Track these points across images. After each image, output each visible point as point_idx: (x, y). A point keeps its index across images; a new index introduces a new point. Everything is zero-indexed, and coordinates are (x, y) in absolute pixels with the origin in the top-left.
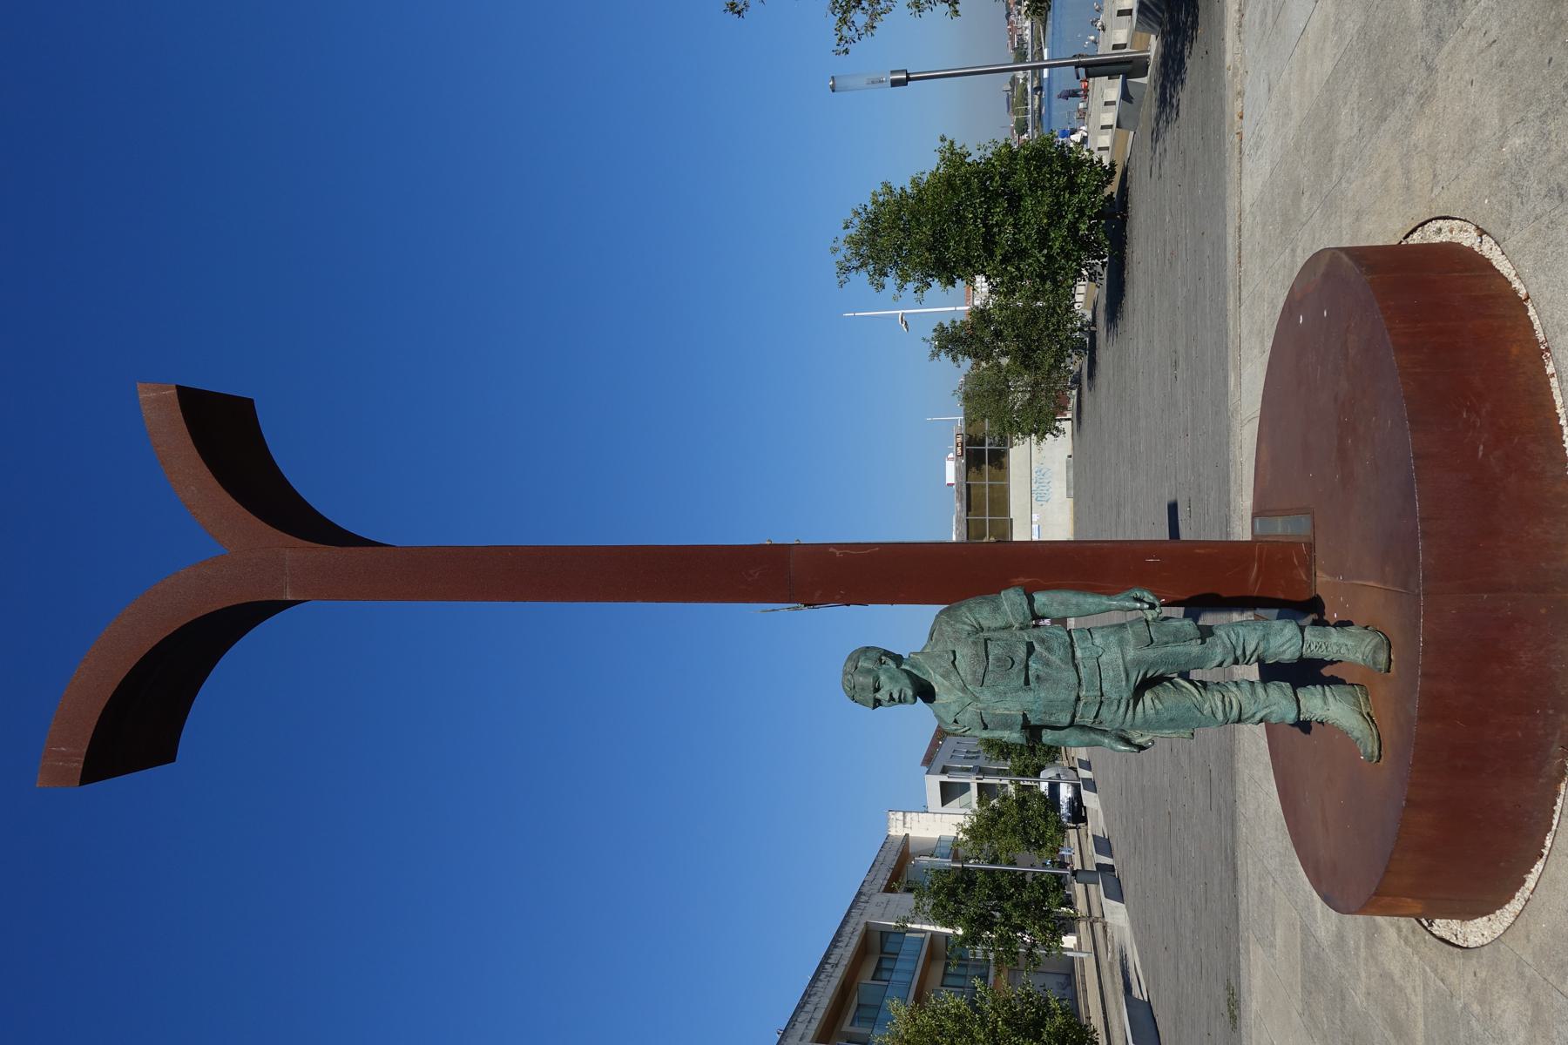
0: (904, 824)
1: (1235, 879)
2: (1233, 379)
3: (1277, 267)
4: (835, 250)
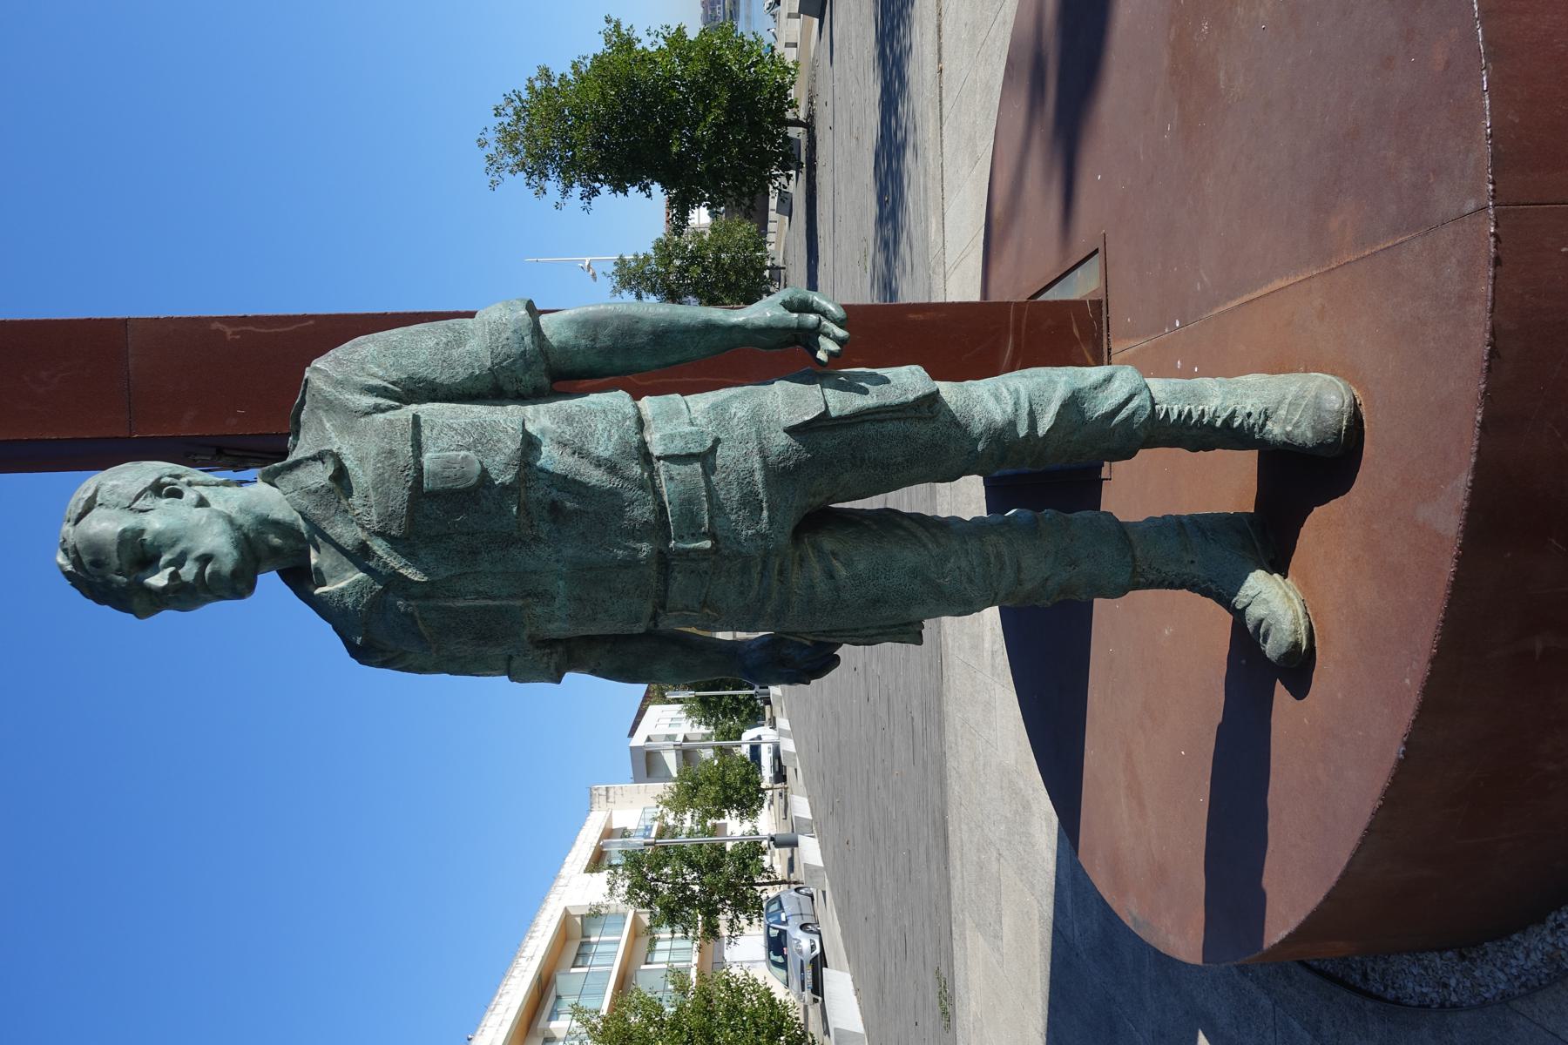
0: (607, 798)
1: (946, 849)
2: (934, 225)
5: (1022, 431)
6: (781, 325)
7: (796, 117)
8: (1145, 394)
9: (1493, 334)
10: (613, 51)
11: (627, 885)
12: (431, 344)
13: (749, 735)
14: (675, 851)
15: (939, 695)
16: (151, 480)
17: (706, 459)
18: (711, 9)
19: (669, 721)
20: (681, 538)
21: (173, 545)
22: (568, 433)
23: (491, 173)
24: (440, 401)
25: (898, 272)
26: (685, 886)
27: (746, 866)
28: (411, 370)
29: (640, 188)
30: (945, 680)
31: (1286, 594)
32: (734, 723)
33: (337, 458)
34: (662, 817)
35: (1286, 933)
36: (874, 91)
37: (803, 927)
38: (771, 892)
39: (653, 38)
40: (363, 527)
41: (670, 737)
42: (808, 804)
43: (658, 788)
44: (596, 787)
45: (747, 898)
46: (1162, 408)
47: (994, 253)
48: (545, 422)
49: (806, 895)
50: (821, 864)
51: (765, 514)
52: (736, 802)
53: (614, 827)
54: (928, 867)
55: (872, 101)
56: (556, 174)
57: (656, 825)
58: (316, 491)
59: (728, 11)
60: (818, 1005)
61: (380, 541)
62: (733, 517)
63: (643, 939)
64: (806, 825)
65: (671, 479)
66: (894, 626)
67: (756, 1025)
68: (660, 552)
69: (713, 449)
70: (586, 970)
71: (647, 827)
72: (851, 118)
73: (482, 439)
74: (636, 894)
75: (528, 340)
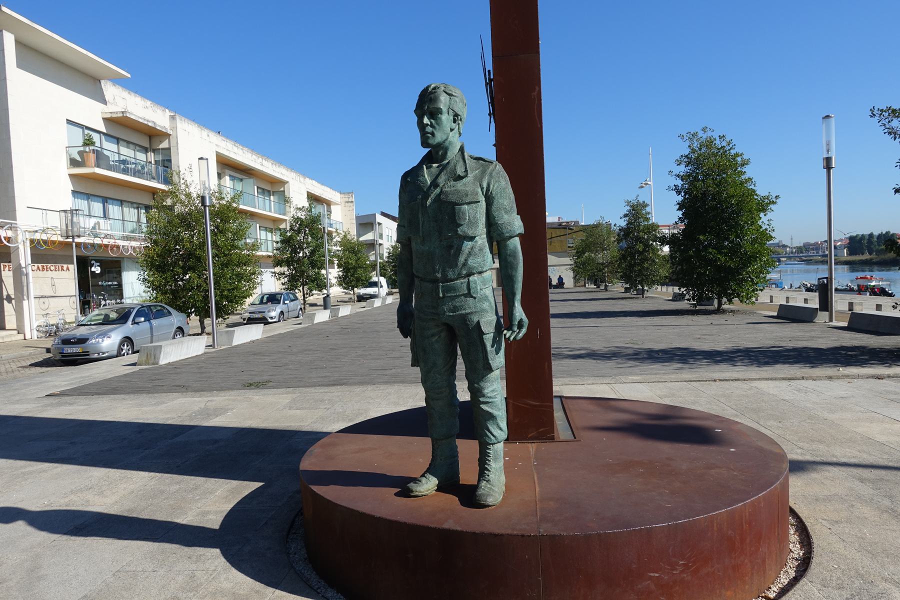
0: (347, 202)
2: (637, 378)
3: (720, 405)
4: (704, 130)
5: (481, 399)
6: (513, 319)
7: (723, 303)
8: (496, 441)
9: (501, 535)
10: (759, 201)
11: (302, 217)
12: (505, 203)
13: (383, 281)
14: (320, 243)
15: (402, 382)
16: (459, 113)
17: (469, 295)
18: (813, 248)
19: (390, 235)
20: (443, 286)
21: (437, 124)
22: (476, 250)
23: (688, 135)
24: (486, 207)
25: (620, 360)
26: (302, 249)
27: (313, 281)
28: (496, 198)
29: (681, 218)
30: (410, 384)
31: (430, 490)
32: (389, 272)
33: (466, 176)
34: (338, 234)
35: (316, 491)
36: (720, 347)
37: (282, 313)
38: (299, 295)
39: (767, 223)
40: (444, 185)
41: (381, 236)
42: (347, 314)
43: (353, 232)
44: (353, 196)
45: (296, 282)
46: (491, 447)
47: (594, 401)
48: (480, 242)
49: (299, 314)
50: (315, 322)
51: (452, 314)
52: (347, 275)
53: (331, 206)
54: (319, 377)
55: (715, 346)
56: (688, 171)
57: (334, 230)
58: (455, 169)
59: (812, 258)
60: (242, 321)
61: (439, 191)
62: (450, 303)
63: (271, 224)
64: (336, 314)
65: (462, 284)
66: (417, 357)
67: (233, 289)
68: (438, 280)
69: (472, 297)
70: (256, 194)
71: (332, 225)
72: (712, 335)
73: (473, 223)
74: (297, 222)
75: (508, 235)
